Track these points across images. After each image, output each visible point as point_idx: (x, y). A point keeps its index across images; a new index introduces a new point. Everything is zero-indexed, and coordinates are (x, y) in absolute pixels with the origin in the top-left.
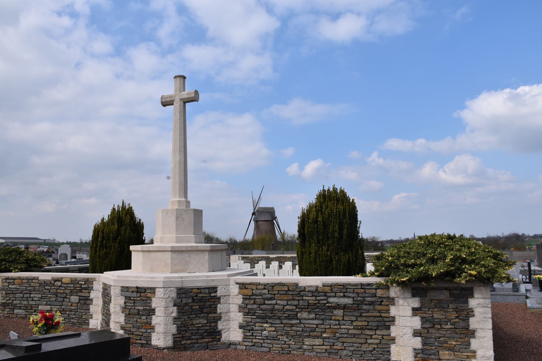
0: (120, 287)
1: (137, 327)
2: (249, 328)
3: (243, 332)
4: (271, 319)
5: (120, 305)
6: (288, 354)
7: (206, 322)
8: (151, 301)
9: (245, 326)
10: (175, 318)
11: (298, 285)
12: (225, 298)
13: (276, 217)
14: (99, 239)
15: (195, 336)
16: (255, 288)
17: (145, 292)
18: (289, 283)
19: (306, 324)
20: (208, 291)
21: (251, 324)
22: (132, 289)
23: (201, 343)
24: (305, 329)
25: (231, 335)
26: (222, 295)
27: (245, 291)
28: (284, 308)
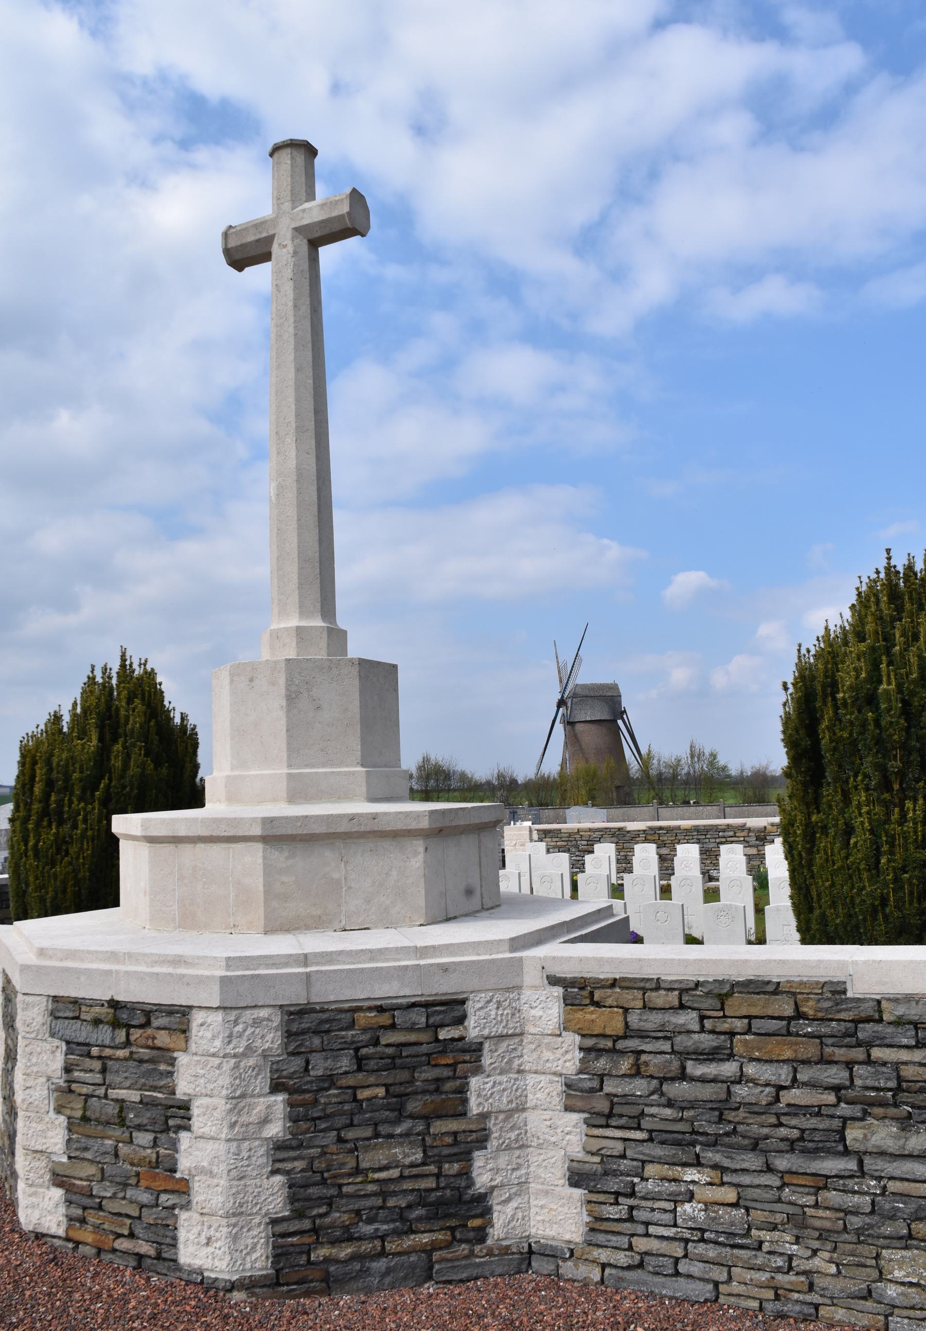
0: (45, 999)
1: (118, 1179)
2: (613, 1184)
3: (589, 1202)
4: (719, 1148)
5: (49, 1079)
6: (805, 1320)
7: (419, 1156)
8: (173, 1065)
9: (595, 1174)
10: (279, 1146)
11: (844, 992)
12: (503, 1046)
13: (625, 711)
14: (37, 790)
15: (370, 1221)
16: (639, 1004)
17: (147, 1024)
18: (801, 983)
19: (891, 1178)
20: (423, 1020)
21: (622, 1167)
22: (93, 1009)
23: (399, 1254)
24: (885, 1204)
25: (533, 1210)
26: (486, 1032)
27: (594, 1016)
28: (777, 1099)
